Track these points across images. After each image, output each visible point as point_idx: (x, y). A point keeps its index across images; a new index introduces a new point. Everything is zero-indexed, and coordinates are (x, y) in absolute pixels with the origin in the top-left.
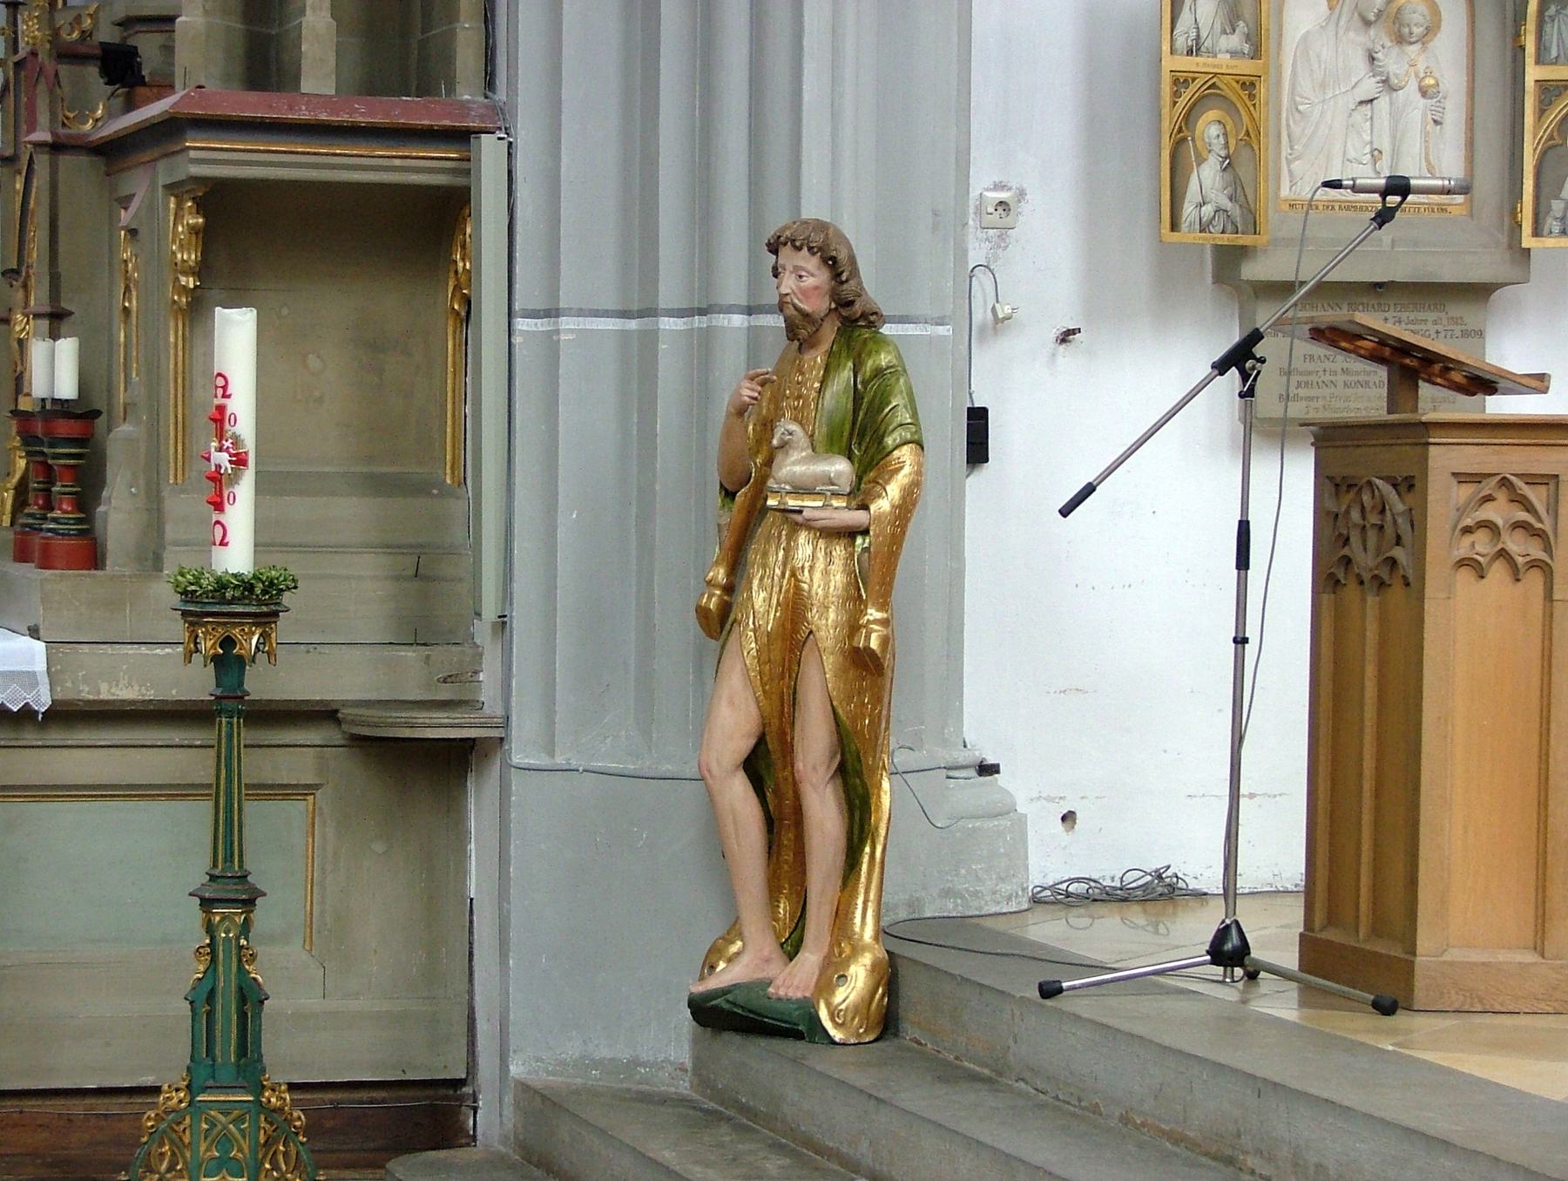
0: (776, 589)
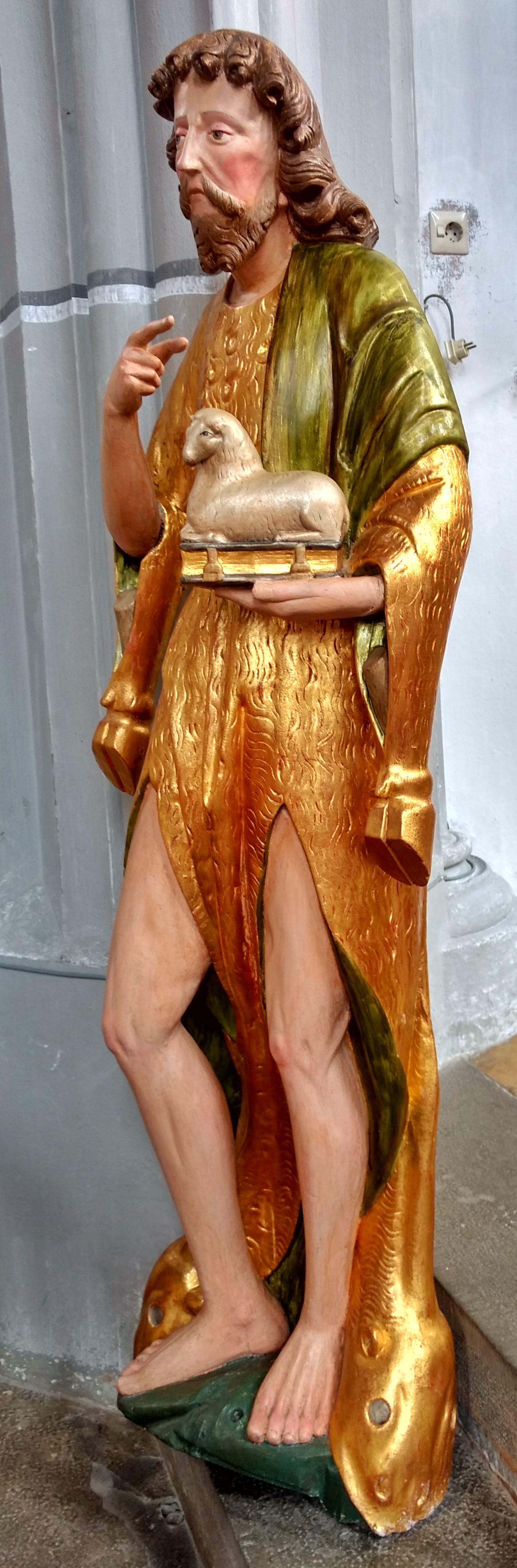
0: (214, 728)
